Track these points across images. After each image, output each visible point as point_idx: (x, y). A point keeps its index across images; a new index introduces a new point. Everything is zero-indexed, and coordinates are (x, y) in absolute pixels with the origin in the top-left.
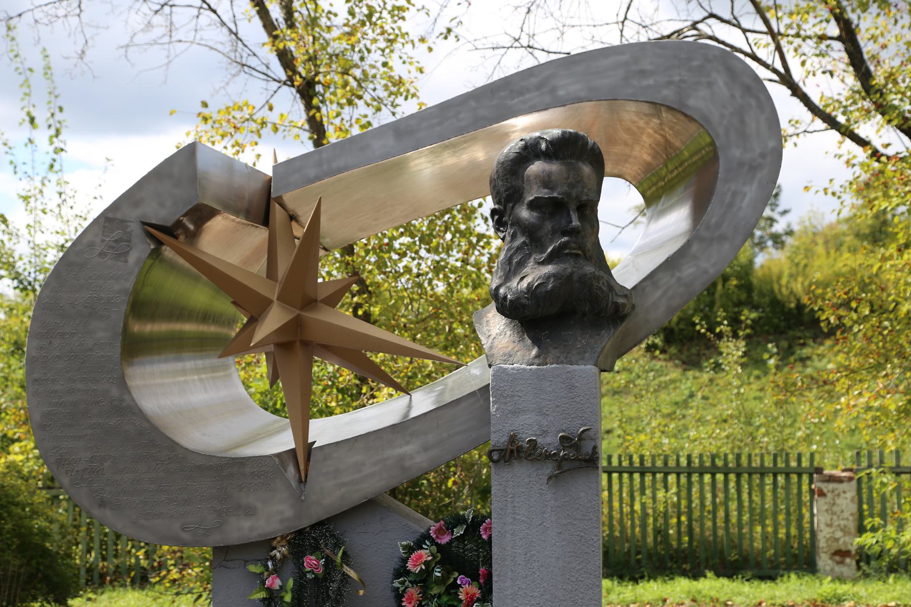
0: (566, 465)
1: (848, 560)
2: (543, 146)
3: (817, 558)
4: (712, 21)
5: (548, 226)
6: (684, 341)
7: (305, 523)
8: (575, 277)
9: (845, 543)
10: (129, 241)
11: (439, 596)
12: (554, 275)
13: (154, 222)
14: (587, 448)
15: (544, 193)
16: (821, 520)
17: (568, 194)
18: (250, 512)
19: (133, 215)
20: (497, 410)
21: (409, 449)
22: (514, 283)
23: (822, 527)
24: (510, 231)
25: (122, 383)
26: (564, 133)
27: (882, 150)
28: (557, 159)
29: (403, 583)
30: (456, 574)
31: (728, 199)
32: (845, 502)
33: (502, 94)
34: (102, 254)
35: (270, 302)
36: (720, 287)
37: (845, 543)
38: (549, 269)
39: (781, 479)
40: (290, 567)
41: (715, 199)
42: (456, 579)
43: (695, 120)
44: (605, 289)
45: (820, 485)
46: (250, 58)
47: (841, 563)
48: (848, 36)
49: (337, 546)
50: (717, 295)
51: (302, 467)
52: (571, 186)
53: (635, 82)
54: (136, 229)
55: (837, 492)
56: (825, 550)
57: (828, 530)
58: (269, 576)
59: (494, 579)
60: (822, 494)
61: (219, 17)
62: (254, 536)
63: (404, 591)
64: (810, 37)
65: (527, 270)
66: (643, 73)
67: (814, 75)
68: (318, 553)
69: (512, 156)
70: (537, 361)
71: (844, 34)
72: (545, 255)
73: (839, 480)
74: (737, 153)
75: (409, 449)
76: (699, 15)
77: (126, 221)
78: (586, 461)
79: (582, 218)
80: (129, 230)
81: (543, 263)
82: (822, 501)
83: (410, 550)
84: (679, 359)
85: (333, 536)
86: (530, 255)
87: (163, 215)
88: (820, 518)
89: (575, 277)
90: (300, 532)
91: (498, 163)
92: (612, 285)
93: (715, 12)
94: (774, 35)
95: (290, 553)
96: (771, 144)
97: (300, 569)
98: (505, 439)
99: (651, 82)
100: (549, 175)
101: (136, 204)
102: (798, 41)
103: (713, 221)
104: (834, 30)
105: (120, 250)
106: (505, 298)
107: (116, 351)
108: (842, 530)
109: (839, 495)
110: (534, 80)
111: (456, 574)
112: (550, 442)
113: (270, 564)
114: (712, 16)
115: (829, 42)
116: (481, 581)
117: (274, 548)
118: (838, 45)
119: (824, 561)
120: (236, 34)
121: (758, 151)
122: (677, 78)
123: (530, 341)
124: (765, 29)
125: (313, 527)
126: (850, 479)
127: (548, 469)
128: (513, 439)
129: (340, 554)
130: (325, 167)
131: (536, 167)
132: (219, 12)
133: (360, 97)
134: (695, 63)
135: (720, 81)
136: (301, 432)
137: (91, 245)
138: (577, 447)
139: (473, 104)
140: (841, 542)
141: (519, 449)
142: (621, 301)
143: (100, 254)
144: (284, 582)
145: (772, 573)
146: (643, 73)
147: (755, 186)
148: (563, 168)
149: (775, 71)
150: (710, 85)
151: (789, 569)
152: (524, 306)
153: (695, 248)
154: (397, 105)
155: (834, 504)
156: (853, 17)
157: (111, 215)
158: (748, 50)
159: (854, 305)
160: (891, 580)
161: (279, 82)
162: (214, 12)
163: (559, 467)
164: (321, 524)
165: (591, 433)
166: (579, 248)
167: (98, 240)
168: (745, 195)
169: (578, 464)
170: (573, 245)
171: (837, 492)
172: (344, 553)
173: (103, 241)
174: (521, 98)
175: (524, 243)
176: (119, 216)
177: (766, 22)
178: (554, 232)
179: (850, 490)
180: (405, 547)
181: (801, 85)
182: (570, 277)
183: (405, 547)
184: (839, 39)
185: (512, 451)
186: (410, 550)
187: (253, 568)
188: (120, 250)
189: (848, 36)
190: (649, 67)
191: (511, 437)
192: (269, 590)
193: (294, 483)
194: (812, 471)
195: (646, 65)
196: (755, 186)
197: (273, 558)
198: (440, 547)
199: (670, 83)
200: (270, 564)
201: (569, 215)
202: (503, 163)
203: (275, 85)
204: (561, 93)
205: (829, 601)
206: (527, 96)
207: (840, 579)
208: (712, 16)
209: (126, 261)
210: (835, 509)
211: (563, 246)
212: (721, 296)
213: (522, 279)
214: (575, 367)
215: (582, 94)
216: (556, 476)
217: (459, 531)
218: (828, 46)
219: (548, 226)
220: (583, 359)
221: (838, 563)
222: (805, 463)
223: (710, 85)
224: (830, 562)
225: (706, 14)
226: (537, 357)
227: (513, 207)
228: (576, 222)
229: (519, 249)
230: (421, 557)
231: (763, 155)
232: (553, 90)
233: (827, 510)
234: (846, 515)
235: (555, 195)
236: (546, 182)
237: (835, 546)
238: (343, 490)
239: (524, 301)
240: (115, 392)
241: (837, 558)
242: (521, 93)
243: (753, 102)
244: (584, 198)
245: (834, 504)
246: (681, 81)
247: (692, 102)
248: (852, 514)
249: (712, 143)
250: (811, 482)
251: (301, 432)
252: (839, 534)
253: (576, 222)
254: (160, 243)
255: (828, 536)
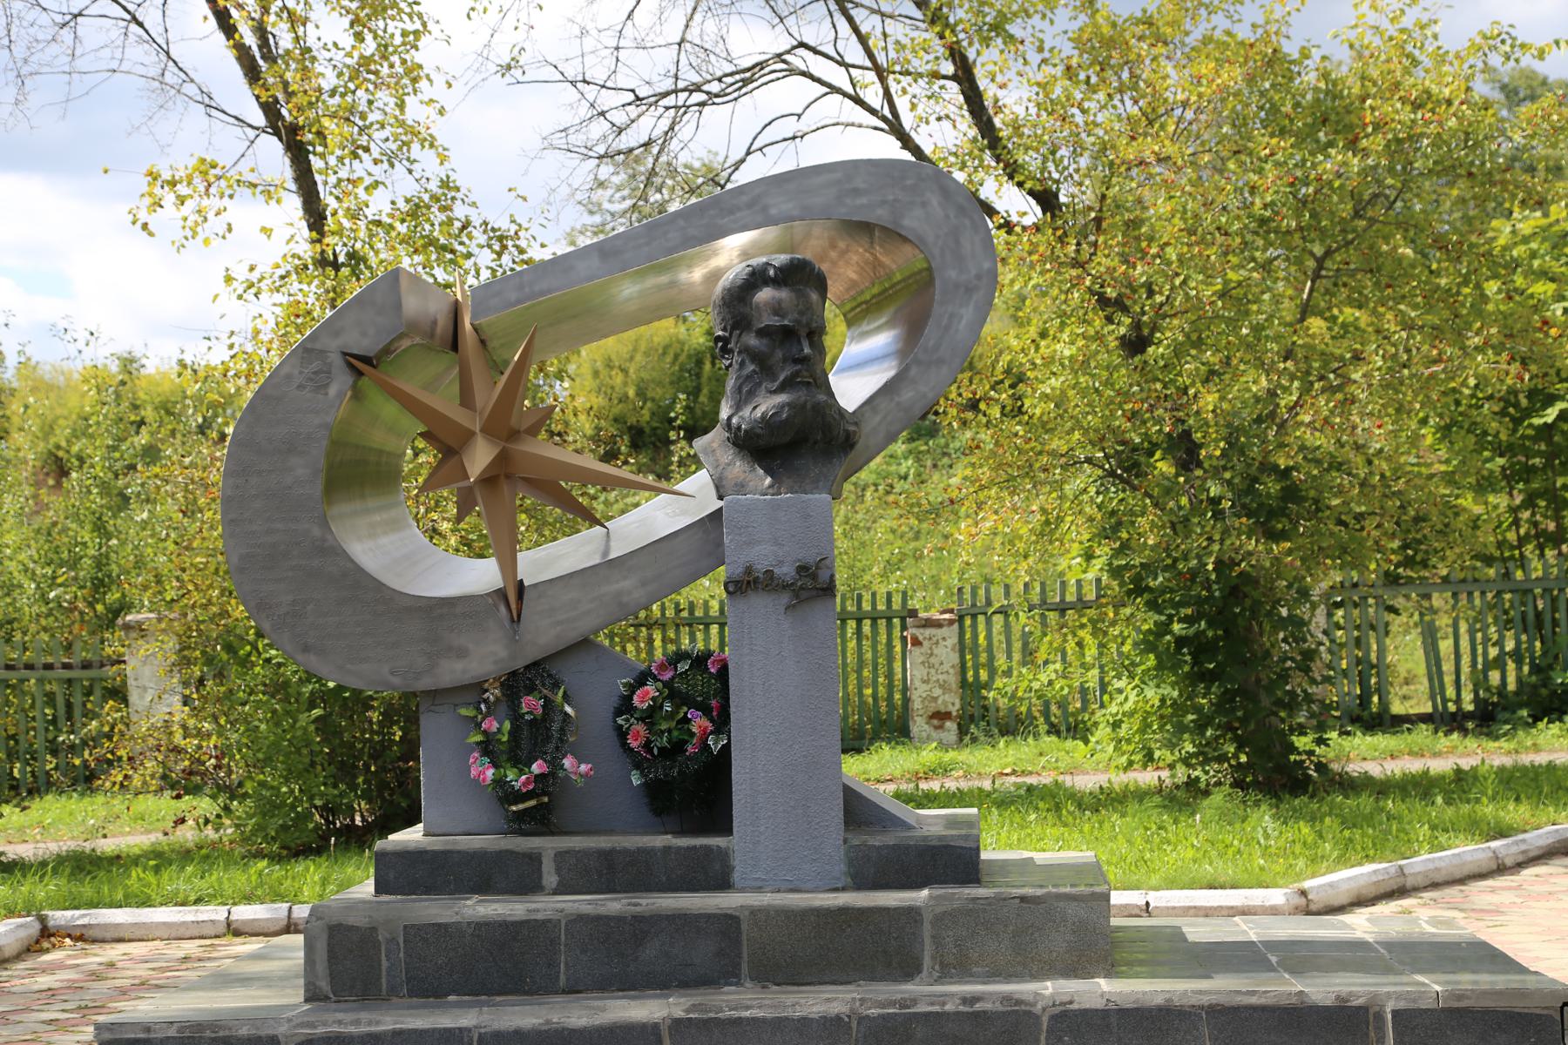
0: (804, 595)
1: (948, 724)
2: (772, 272)
3: (911, 723)
4: (801, 51)
5: (779, 354)
6: (658, 444)
7: (519, 664)
8: (809, 406)
9: (945, 703)
10: (330, 373)
11: (669, 731)
12: (789, 404)
13: (355, 352)
14: (823, 576)
15: (775, 321)
16: (915, 673)
17: (798, 322)
18: (462, 653)
19: (333, 345)
20: (731, 541)
21: (626, 584)
22: (746, 412)
23: (917, 683)
24: (737, 358)
25: (324, 523)
26: (792, 260)
27: (1014, 219)
28: (786, 285)
29: (627, 720)
30: (685, 709)
31: (945, 322)
32: (945, 650)
33: (712, 212)
34: (301, 387)
35: (472, 434)
36: (707, 366)
37: (945, 703)
38: (782, 398)
39: (867, 627)
40: (503, 709)
41: (931, 322)
42: (686, 713)
43: (910, 241)
44: (837, 416)
45: (914, 631)
46: (185, 85)
47: (940, 727)
48: (965, 76)
49: (556, 685)
50: (704, 379)
51: (513, 606)
52: (801, 313)
53: (848, 201)
54: (337, 361)
55: (935, 639)
56: (920, 712)
57: (925, 687)
58: (483, 719)
59: (732, 709)
60: (917, 642)
61: (147, 32)
62: (467, 679)
63: (628, 728)
64: (921, 75)
65: (758, 400)
66: (856, 192)
67: (927, 123)
68: (536, 693)
69: (739, 282)
70: (771, 491)
71: (960, 73)
72: (777, 384)
73: (938, 624)
74: (952, 274)
75: (626, 584)
76: (785, 43)
77: (325, 352)
78: (822, 589)
79: (812, 345)
80: (329, 360)
81: (775, 392)
82: (917, 651)
83: (632, 688)
84: (652, 472)
85: (550, 676)
86: (760, 384)
87: (365, 344)
88: (915, 672)
89: (809, 406)
90: (513, 674)
91: (724, 289)
92: (841, 412)
93: (805, 40)
94: (881, 74)
95: (503, 694)
96: (987, 265)
97: (515, 711)
98: (740, 570)
99: (864, 200)
100: (780, 302)
101: (337, 334)
102: (906, 80)
103: (931, 343)
104: (948, 68)
105: (319, 382)
106: (739, 428)
107: (318, 488)
108: (941, 686)
109: (937, 643)
110: (745, 198)
111: (685, 709)
112: (786, 571)
113: (483, 706)
114: (802, 45)
115: (942, 82)
116: (715, 714)
117: (486, 691)
118: (953, 87)
119: (919, 726)
120: (167, 53)
121: (974, 272)
122: (891, 198)
123: (762, 471)
124: (868, 64)
125: (527, 667)
126: (951, 622)
127: (785, 598)
128: (749, 570)
129: (561, 693)
130: (527, 290)
131: (765, 295)
132: (147, 25)
133: (367, 150)
134: (909, 182)
135: (934, 200)
136: (508, 564)
137: (289, 377)
138: (814, 577)
139: (681, 223)
140: (940, 701)
141: (756, 580)
142: (852, 428)
143: (299, 387)
144: (501, 724)
145: (856, 744)
146: (856, 192)
147: (971, 308)
148: (793, 295)
149: (884, 119)
150: (924, 204)
151: (876, 737)
152: (758, 436)
153: (913, 371)
154: (415, 161)
155: (931, 654)
156: (971, 54)
157: (309, 346)
158: (850, 90)
159: (982, 406)
160: (1002, 744)
161: (257, 129)
162: (141, 25)
163: (797, 596)
164: (536, 664)
165: (827, 562)
166: (811, 376)
167: (296, 372)
168: (962, 317)
169: (814, 593)
170: (805, 373)
171: (935, 639)
172: (565, 692)
173: (301, 373)
174: (732, 217)
175: (754, 371)
176: (318, 346)
177: (870, 54)
178: (785, 360)
179: (950, 635)
180: (625, 685)
181: (913, 134)
182: (804, 406)
183: (625, 685)
184: (954, 78)
185: (749, 582)
186: (632, 688)
187: (464, 712)
188: (319, 382)
189: (965, 76)
190: (862, 186)
191: (747, 568)
192: (485, 733)
193: (507, 623)
194: (905, 614)
195: (859, 183)
196: (971, 308)
197: (486, 701)
198: (665, 684)
199: (884, 202)
200: (483, 706)
201: (799, 342)
202: (729, 290)
203: (251, 133)
204: (773, 211)
205: (933, 771)
206: (739, 215)
207: (943, 746)
208: (802, 45)
209: (327, 394)
210: (932, 660)
211: (796, 374)
212: (710, 379)
213: (755, 408)
214: (810, 496)
215: (796, 213)
216: (794, 606)
217: (683, 667)
218: (942, 87)
219: (779, 354)
220: (817, 488)
221: (936, 728)
222: (896, 605)
223: (924, 204)
224: (926, 727)
225: (795, 43)
226: (771, 486)
227: (740, 335)
228: (807, 350)
229: (749, 378)
230: (648, 693)
231: (978, 277)
232: (765, 209)
233: (923, 663)
234: (946, 667)
235: (786, 322)
236: (777, 309)
237: (932, 708)
238: (559, 628)
239: (759, 431)
240: (316, 532)
241: (935, 722)
242: (731, 212)
243: (967, 222)
244: (814, 325)
245: (931, 654)
246: (895, 200)
247: (906, 222)
248: (953, 666)
249: (929, 269)
250: (904, 627)
251: (508, 564)
252: (937, 692)
253: (807, 350)
254: (360, 374)
255: (924, 695)
